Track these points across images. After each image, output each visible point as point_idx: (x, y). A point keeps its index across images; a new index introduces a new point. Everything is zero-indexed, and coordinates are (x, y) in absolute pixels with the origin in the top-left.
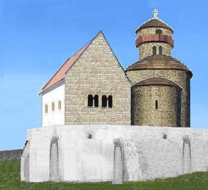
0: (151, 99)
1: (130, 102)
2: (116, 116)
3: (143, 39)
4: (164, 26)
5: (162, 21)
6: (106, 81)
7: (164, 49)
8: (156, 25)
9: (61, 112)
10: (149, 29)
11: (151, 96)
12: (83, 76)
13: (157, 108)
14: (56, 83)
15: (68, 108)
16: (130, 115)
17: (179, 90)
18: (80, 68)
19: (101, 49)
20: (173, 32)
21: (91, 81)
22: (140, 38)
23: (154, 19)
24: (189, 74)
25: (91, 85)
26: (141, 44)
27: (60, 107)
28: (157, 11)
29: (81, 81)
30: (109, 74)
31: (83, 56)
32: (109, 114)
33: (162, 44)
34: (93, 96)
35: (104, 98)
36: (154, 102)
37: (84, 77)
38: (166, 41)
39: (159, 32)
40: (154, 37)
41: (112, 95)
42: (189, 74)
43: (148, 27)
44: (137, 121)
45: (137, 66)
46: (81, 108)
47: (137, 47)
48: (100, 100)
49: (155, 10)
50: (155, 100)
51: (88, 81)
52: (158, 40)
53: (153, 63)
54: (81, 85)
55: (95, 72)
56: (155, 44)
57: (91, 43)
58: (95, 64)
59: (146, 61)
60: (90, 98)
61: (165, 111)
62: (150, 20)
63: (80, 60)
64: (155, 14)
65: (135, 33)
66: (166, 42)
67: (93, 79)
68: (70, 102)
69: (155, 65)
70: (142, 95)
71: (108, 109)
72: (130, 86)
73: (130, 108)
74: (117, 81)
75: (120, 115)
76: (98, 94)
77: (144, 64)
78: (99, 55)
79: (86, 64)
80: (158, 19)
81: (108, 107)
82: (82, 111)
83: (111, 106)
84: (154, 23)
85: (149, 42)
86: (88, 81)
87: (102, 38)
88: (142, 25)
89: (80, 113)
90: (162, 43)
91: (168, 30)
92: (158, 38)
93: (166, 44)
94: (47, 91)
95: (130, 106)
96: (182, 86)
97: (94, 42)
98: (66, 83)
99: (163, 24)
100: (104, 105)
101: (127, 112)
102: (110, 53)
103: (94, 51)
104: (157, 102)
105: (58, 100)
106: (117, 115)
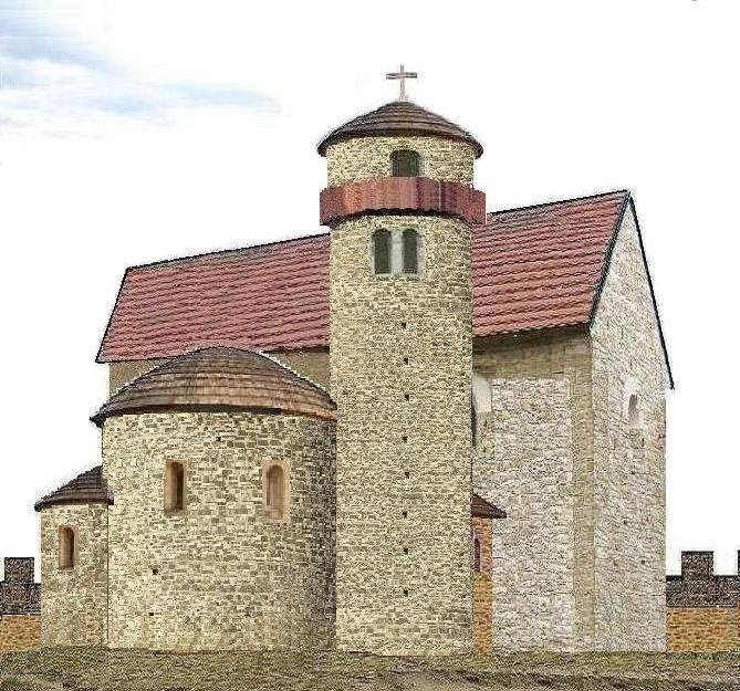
4: (459, 134)
33: (427, 227)
38: (448, 208)
39: (405, 163)
45: (137, 395)
52: (414, 206)
53: (200, 383)
56: (379, 222)
59: (172, 377)
66: (445, 215)
69: (206, 391)
77: (162, 388)
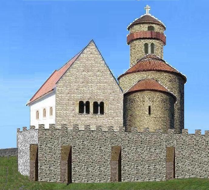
0: (144, 105)
1: (123, 108)
2: (108, 122)
3: (135, 36)
4: (156, 22)
5: (154, 18)
6: (98, 91)
7: (156, 46)
8: (148, 21)
9: (52, 118)
10: (141, 25)
11: (144, 101)
12: (74, 86)
13: (150, 113)
14: (45, 94)
15: (59, 114)
16: (122, 121)
17: (172, 98)
18: (71, 78)
19: (93, 58)
20: (165, 28)
21: (82, 91)
22: (132, 34)
23: (146, 16)
24: (182, 79)
25: (82, 95)
26: (133, 40)
27: (51, 114)
28: (149, 7)
29: (72, 91)
30: (101, 85)
31: (75, 65)
32: (101, 120)
33: (153, 41)
34: (85, 102)
35: (95, 104)
36: (146, 107)
37: (75, 87)
39: (151, 29)
40: (146, 33)
41: (104, 101)
42: (182, 79)
43: (140, 23)
44: (130, 120)
46: (72, 114)
47: (128, 44)
48: (91, 106)
49: (148, 6)
50: (148, 105)
51: (79, 91)
52: (150, 37)
54: (72, 95)
55: (86, 82)
56: (147, 41)
57: (82, 52)
58: (86, 74)
60: (81, 104)
61: (158, 117)
62: (142, 16)
63: (71, 70)
64: (147, 10)
65: (128, 30)
66: (158, 39)
67: (85, 89)
68: (61, 108)
70: (135, 101)
71: (100, 116)
72: (123, 95)
73: (122, 114)
74: (109, 91)
75: (112, 121)
76: (90, 101)
78: (91, 64)
79: (77, 74)
80: (150, 15)
81: (99, 113)
82: (73, 117)
83: (102, 112)
84: (146, 20)
85: (140, 39)
86: (79, 91)
87: (94, 47)
88: (134, 21)
89: (72, 118)
90: (154, 40)
91: (160, 27)
92: (150, 34)
93: (157, 41)
94: (35, 102)
95: (122, 111)
96: (176, 95)
97: (85, 51)
98: (57, 93)
99: (155, 20)
100: (95, 112)
101: (119, 118)
102: (102, 62)
103: (85, 60)
104: (150, 107)
105: (50, 106)
106: (109, 121)
